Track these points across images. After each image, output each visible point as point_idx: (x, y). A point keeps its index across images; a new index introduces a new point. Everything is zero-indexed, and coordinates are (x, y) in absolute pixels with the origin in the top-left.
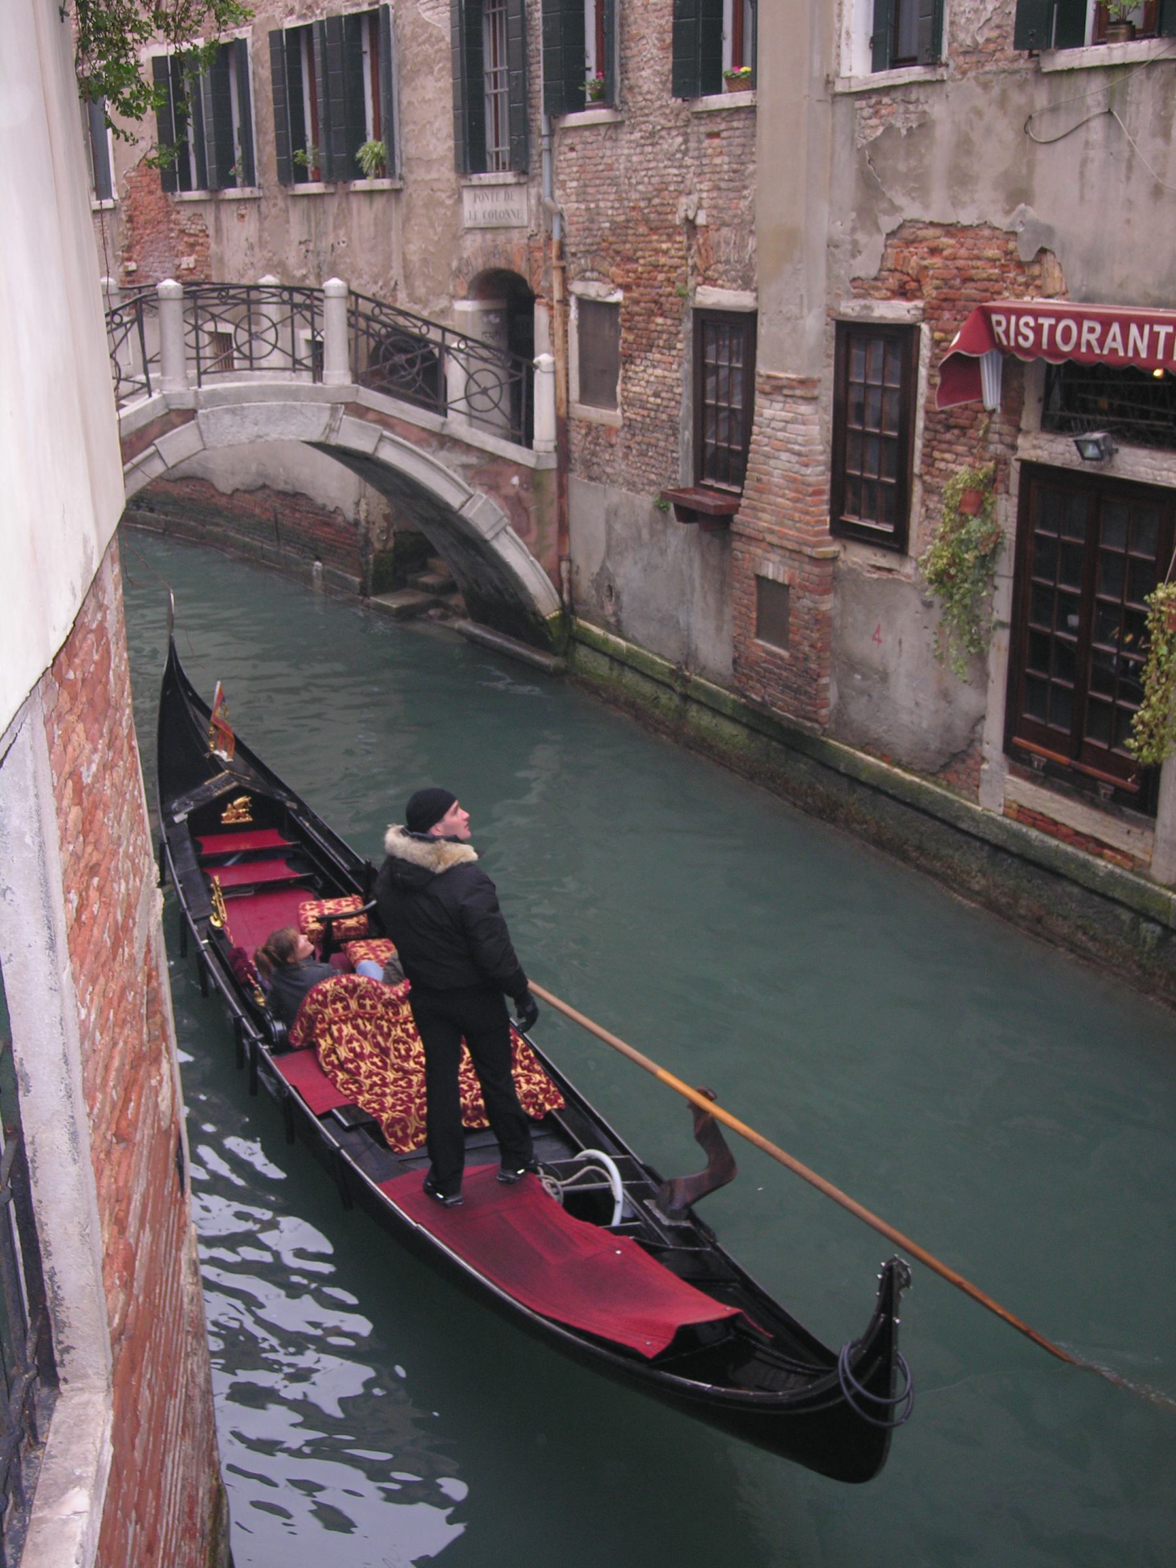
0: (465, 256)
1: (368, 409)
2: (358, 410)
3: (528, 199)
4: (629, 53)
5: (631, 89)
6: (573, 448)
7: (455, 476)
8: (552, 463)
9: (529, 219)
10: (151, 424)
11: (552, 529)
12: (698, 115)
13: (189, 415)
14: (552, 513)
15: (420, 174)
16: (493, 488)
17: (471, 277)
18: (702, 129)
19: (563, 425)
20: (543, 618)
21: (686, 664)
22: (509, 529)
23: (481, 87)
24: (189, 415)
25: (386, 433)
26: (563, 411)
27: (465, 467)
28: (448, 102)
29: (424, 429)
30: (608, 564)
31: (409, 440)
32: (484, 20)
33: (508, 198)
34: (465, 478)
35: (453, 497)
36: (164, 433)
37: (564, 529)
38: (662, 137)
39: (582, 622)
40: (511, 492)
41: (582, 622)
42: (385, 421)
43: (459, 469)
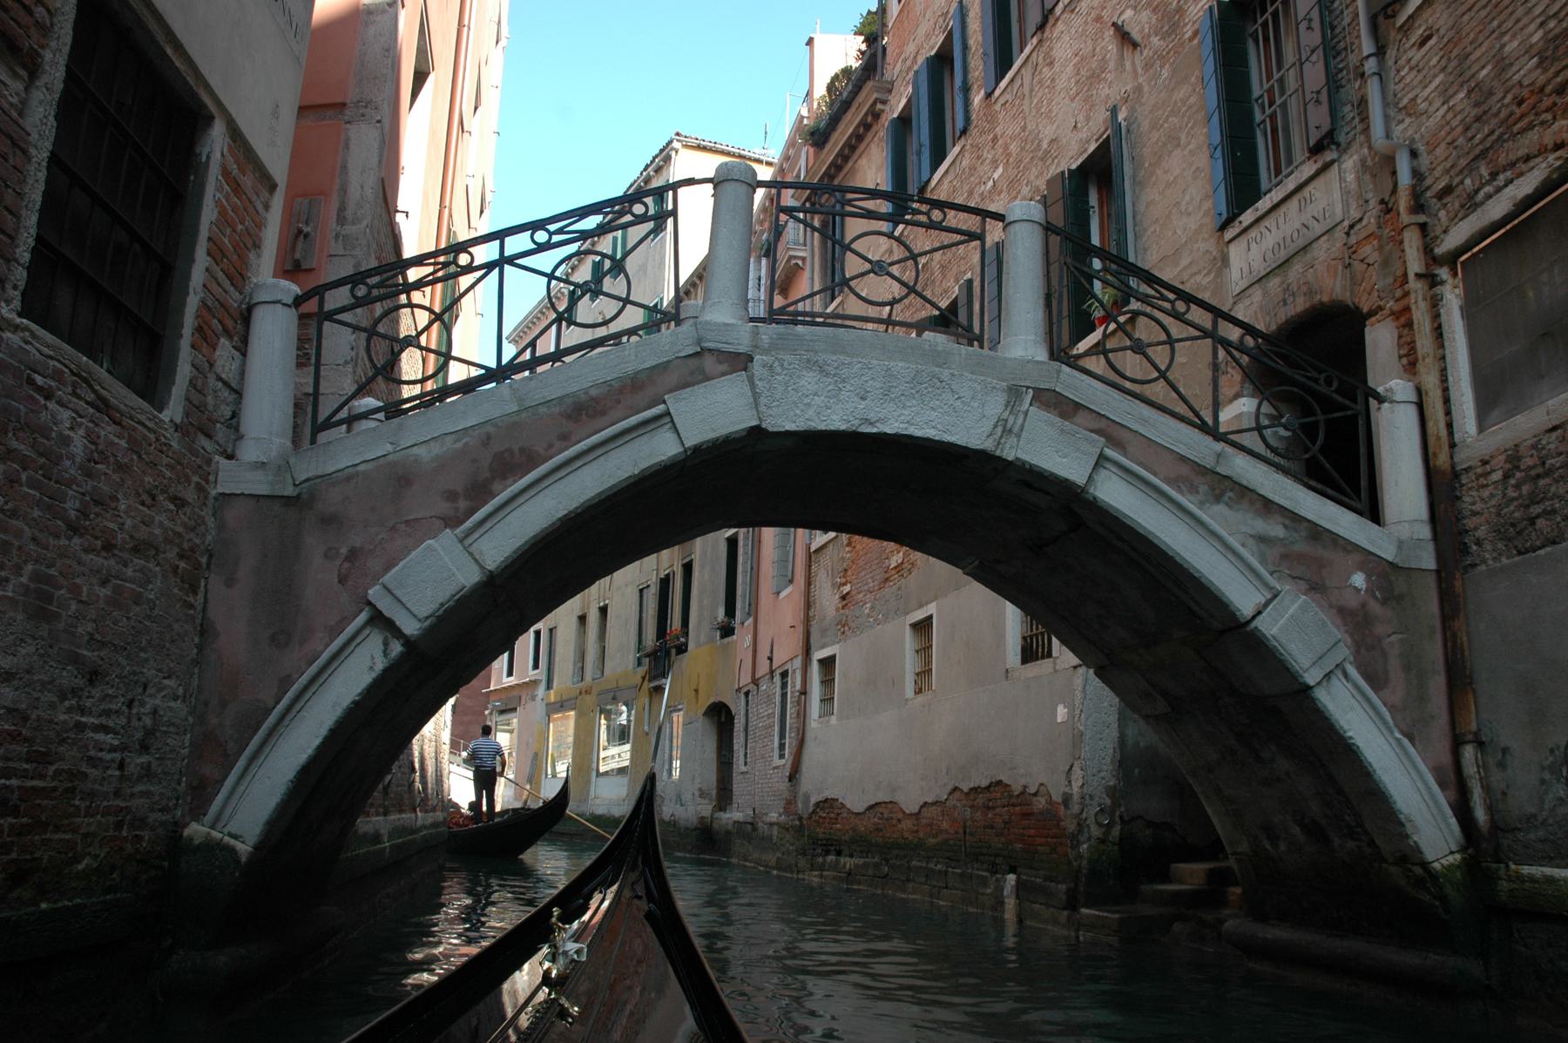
1: (1078, 406)
7: (1242, 550)
8: (1428, 561)
10: (664, 367)
11: (1437, 685)
13: (740, 362)
14: (1435, 651)
16: (1316, 588)
19: (1442, 486)
20: (1425, 865)
22: (1352, 671)
24: (740, 362)
25: (1109, 452)
27: (1262, 539)
29: (1183, 459)
34: (1263, 562)
35: (1242, 596)
40: (1352, 602)
42: (1111, 432)
43: (1251, 542)
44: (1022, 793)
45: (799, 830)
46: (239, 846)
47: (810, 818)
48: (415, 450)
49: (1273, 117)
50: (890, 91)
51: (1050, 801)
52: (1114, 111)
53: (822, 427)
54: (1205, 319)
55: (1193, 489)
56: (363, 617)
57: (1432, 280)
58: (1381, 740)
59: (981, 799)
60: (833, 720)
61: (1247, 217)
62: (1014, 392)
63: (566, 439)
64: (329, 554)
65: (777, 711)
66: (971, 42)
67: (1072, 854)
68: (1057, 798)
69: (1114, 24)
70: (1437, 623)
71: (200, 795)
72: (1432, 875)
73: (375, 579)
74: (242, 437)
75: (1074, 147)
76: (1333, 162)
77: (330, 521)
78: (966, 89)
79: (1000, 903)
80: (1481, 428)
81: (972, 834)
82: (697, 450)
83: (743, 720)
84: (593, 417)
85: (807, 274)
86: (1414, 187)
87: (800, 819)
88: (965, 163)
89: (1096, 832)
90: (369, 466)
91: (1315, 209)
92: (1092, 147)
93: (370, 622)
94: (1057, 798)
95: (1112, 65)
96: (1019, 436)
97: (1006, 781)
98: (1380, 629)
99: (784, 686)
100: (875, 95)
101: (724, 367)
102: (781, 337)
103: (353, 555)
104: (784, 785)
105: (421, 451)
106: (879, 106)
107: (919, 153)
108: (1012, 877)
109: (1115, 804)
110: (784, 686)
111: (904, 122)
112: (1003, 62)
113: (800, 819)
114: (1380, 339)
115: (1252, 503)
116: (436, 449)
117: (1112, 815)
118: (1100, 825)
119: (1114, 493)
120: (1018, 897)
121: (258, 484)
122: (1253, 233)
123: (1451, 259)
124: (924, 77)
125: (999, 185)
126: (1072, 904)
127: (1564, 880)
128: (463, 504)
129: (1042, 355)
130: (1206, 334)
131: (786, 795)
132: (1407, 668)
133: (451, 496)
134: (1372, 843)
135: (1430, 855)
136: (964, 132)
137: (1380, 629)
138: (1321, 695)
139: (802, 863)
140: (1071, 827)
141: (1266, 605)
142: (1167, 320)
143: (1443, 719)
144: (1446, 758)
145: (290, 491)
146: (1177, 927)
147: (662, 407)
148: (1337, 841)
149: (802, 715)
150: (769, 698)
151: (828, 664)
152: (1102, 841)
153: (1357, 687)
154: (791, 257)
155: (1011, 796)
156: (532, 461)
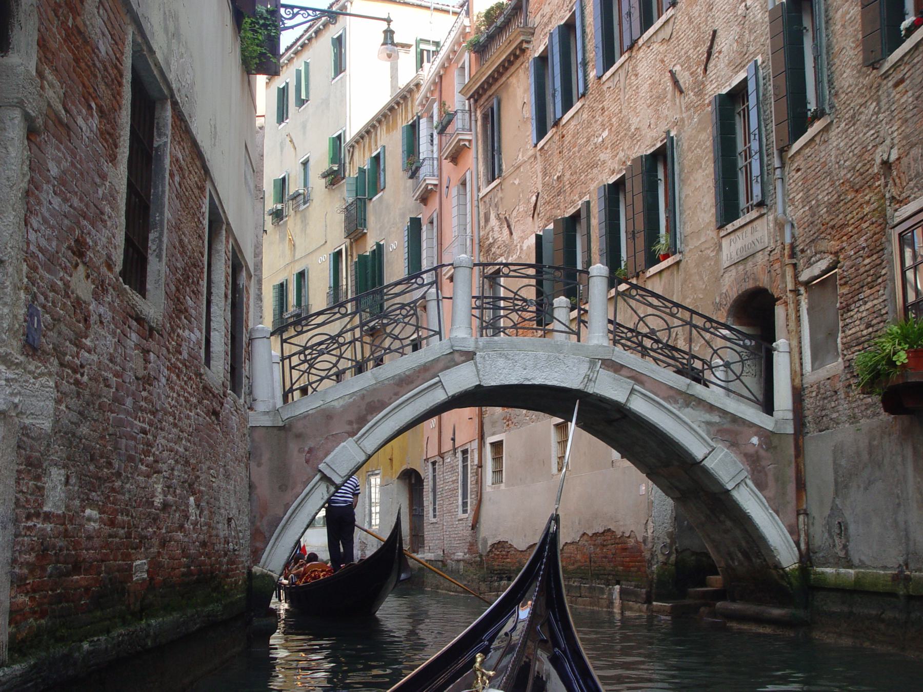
0: (724, 291)
1: (622, 366)
2: (615, 367)
3: (768, 224)
4: (833, 68)
5: (836, 94)
6: (807, 413)
7: (698, 429)
8: (790, 429)
9: (769, 239)
10: (437, 360)
11: (791, 488)
12: (886, 76)
13: (470, 356)
14: (791, 472)
15: (693, 243)
16: (733, 444)
17: (727, 308)
18: (890, 84)
19: (798, 394)
20: (783, 569)
21: (907, 565)
22: (749, 482)
23: (734, 164)
24: (470, 356)
25: (636, 387)
26: (797, 381)
27: (708, 423)
28: (711, 183)
29: (671, 388)
30: (838, 502)
31: (658, 396)
32: (737, 117)
33: (754, 230)
34: (708, 434)
35: (698, 450)
36: (448, 368)
37: (801, 486)
38: (861, 113)
39: (819, 570)
40: (751, 450)
41: (819, 570)
42: (637, 378)
43: (703, 425)
44: (622, 536)
45: (480, 564)
46: (274, 575)
47: (488, 555)
48: (333, 403)
49: (746, 166)
50: (533, 34)
51: (637, 542)
52: (668, 132)
53: (507, 383)
54: (687, 315)
55: (676, 402)
56: (318, 477)
57: (796, 292)
58: (763, 514)
59: (599, 540)
60: (503, 486)
61: (730, 227)
62: (593, 362)
63: (397, 395)
64: (301, 451)
65: (460, 478)
66: (588, 30)
67: (648, 571)
68: (640, 539)
69: (671, 71)
70: (793, 459)
71: (256, 554)
72: (786, 574)
73: (321, 461)
74: (254, 400)
75: (648, 142)
76: (764, 214)
77: (299, 436)
78: (585, 64)
79: (611, 603)
80: (813, 369)
81: (595, 562)
82: (453, 396)
83: (431, 483)
84: (407, 384)
85: (472, 154)
86: (792, 244)
87: (481, 556)
88: (585, 116)
89: (661, 558)
90: (314, 411)
91: (758, 235)
92: (659, 145)
93: (321, 479)
94: (640, 539)
95: (669, 96)
96: (595, 382)
97: (613, 529)
98: (763, 463)
99: (465, 460)
100: (522, 38)
101: (463, 358)
102: (488, 342)
103: (310, 451)
104: (468, 532)
105: (335, 404)
106: (525, 45)
107: (554, 96)
108: (617, 587)
109: (673, 542)
110: (465, 460)
111: (543, 61)
112: (609, 61)
113: (481, 556)
114: (780, 312)
115: (704, 406)
116: (342, 402)
117: (671, 547)
118: (662, 553)
119: (640, 406)
120: (621, 599)
121: (266, 421)
122: (732, 237)
123: (807, 284)
124: (556, 39)
125: (606, 142)
126: (648, 601)
127: (920, 578)
128: (355, 426)
129: (605, 342)
130: (687, 323)
131: (469, 539)
132: (777, 480)
133: (350, 423)
134: (765, 560)
135: (784, 565)
136: (583, 95)
137: (763, 463)
138: (736, 495)
139: (483, 587)
140: (647, 555)
141: (709, 454)
142: (667, 318)
143: (794, 502)
144: (793, 521)
145: (281, 424)
146: (702, 609)
147: (437, 378)
148: (754, 559)
149: (479, 482)
150: (453, 469)
151: (497, 447)
152: (665, 564)
153: (751, 490)
154: (460, 140)
155: (616, 538)
156: (383, 405)
